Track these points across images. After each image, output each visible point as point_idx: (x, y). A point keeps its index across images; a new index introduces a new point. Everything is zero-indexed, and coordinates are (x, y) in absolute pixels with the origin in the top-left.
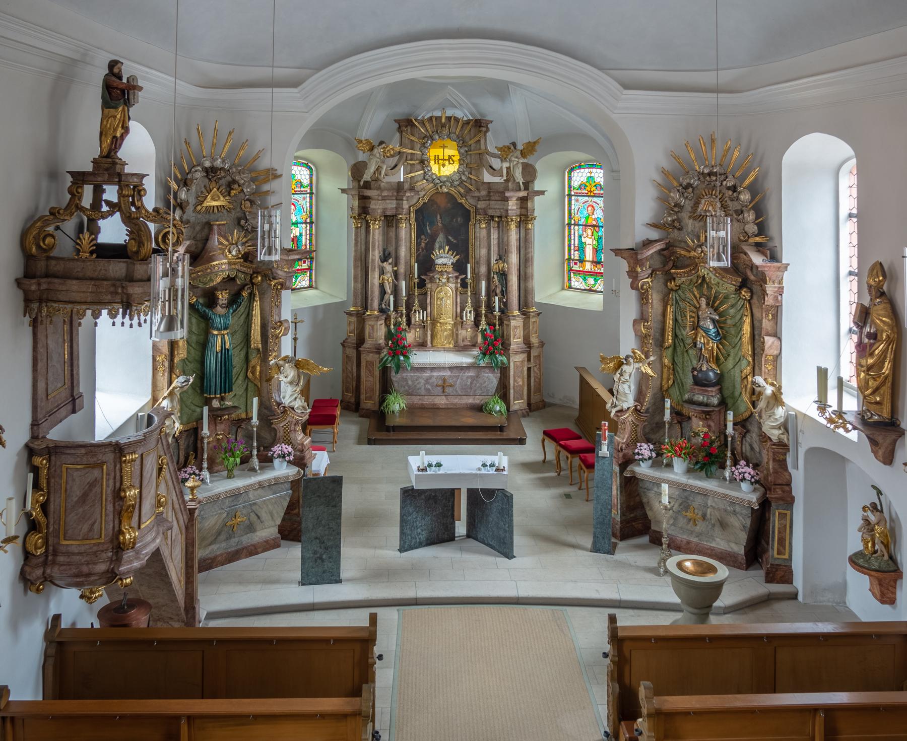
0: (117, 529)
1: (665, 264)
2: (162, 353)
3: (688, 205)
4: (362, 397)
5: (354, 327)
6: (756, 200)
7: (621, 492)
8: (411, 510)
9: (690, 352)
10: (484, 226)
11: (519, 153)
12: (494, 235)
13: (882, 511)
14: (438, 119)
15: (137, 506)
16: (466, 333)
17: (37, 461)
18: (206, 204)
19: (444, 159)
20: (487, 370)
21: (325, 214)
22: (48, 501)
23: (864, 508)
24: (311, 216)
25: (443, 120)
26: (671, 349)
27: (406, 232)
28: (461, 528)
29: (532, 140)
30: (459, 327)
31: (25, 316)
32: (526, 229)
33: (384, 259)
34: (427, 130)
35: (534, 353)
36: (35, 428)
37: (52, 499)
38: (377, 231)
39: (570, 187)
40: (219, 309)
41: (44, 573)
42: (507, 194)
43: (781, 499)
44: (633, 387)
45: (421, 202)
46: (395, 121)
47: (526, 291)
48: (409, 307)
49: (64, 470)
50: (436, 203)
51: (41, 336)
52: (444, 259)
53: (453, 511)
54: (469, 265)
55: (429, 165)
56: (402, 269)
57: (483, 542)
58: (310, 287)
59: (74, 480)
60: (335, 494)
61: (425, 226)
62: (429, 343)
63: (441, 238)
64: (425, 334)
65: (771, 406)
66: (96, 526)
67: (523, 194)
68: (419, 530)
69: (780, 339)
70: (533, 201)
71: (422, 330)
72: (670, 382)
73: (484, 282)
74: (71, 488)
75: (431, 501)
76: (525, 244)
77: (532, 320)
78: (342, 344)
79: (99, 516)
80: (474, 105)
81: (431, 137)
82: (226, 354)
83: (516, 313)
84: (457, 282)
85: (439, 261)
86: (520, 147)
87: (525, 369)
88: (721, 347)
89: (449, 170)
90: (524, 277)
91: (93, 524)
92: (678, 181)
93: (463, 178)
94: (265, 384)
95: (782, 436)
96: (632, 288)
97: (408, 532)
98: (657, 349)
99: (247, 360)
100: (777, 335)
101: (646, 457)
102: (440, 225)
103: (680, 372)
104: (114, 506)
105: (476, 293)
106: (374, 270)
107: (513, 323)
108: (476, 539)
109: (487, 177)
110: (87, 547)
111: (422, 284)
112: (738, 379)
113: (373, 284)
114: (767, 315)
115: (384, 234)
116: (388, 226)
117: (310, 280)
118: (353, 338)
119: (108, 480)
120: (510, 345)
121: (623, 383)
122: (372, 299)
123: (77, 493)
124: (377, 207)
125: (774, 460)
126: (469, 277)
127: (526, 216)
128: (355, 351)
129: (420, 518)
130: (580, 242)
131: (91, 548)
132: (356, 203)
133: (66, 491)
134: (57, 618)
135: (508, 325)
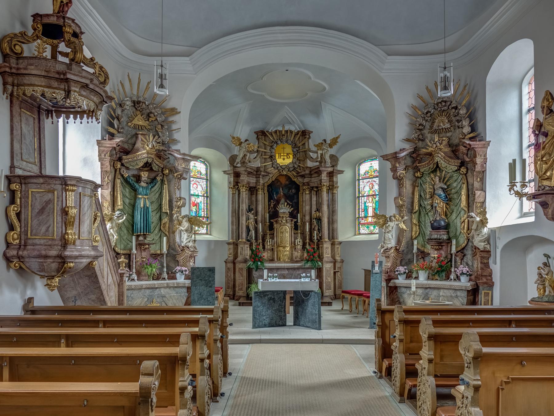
0: (64, 232)
1: (413, 162)
2: (106, 201)
3: (428, 125)
4: (237, 289)
5: (232, 251)
6: (470, 111)
7: (387, 298)
8: (259, 304)
9: (429, 214)
10: (307, 192)
11: (328, 145)
12: (314, 199)
13: (549, 266)
15: (77, 218)
16: (297, 254)
17: (14, 186)
18: (133, 122)
21: (215, 192)
22: (20, 211)
23: (539, 268)
24: (207, 193)
25: (283, 133)
26: (418, 213)
27: (262, 197)
28: (290, 319)
30: (294, 250)
31: (4, 94)
32: (333, 194)
33: (250, 210)
34: (274, 139)
35: (338, 265)
36: (12, 169)
37: (23, 211)
39: (359, 174)
40: (143, 184)
41: (17, 253)
42: (321, 169)
43: (485, 283)
44: (394, 236)
45: (271, 181)
46: (255, 132)
47: (333, 230)
48: (264, 240)
49: (30, 192)
50: (280, 181)
51: (16, 125)
52: (284, 209)
53: (285, 308)
54: (299, 215)
56: (259, 218)
57: (303, 326)
58: (207, 234)
59: (36, 199)
60: (211, 279)
62: (276, 259)
63: (283, 200)
65: (479, 228)
66: (51, 228)
67: (330, 169)
68: (264, 318)
69: (485, 192)
70: (337, 177)
72: (418, 234)
73: (308, 224)
74: (34, 204)
76: (332, 203)
77: (336, 246)
79: (52, 223)
80: (302, 122)
81: (276, 143)
82: (146, 209)
83: (327, 240)
84: (292, 224)
85: (281, 211)
86: (328, 142)
87: (332, 272)
88: (448, 207)
89: (288, 161)
90: (332, 221)
91: (49, 227)
92: (421, 112)
93: (296, 166)
94: (171, 235)
95: (486, 246)
96: (394, 179)
97: (257, 317)
98: (409, 215)
99: (160, 219)
100: (483, 189)
101: (402, 272)
102: (282, 194)
103: (423, 227)
104: (62, 219)
106: (242, 215)
107: (325, 245)
108: (300, 326)
109: (310, 164)
110: (45, 241)
111: (271, 227)
112: (459, 224)
113: (242, 224)
114: (477, 179)
115: (249, 199)
116: (251, 194)
117: (207, 229)
118: (231, 258)
119: (58, 201)
121: (388, 232)
122: (242, 233)
123: (38, 207)
124: (244, 178)
125: (481, 263)
126: (299, 221)
127: (333, 186)
128: (232, 264)
129: (265, 310)
130: (365, 206)
131: (47, 242)
132: (232, 179)
133: (31, 206)
134: (30, 300)
135: (321, 247)
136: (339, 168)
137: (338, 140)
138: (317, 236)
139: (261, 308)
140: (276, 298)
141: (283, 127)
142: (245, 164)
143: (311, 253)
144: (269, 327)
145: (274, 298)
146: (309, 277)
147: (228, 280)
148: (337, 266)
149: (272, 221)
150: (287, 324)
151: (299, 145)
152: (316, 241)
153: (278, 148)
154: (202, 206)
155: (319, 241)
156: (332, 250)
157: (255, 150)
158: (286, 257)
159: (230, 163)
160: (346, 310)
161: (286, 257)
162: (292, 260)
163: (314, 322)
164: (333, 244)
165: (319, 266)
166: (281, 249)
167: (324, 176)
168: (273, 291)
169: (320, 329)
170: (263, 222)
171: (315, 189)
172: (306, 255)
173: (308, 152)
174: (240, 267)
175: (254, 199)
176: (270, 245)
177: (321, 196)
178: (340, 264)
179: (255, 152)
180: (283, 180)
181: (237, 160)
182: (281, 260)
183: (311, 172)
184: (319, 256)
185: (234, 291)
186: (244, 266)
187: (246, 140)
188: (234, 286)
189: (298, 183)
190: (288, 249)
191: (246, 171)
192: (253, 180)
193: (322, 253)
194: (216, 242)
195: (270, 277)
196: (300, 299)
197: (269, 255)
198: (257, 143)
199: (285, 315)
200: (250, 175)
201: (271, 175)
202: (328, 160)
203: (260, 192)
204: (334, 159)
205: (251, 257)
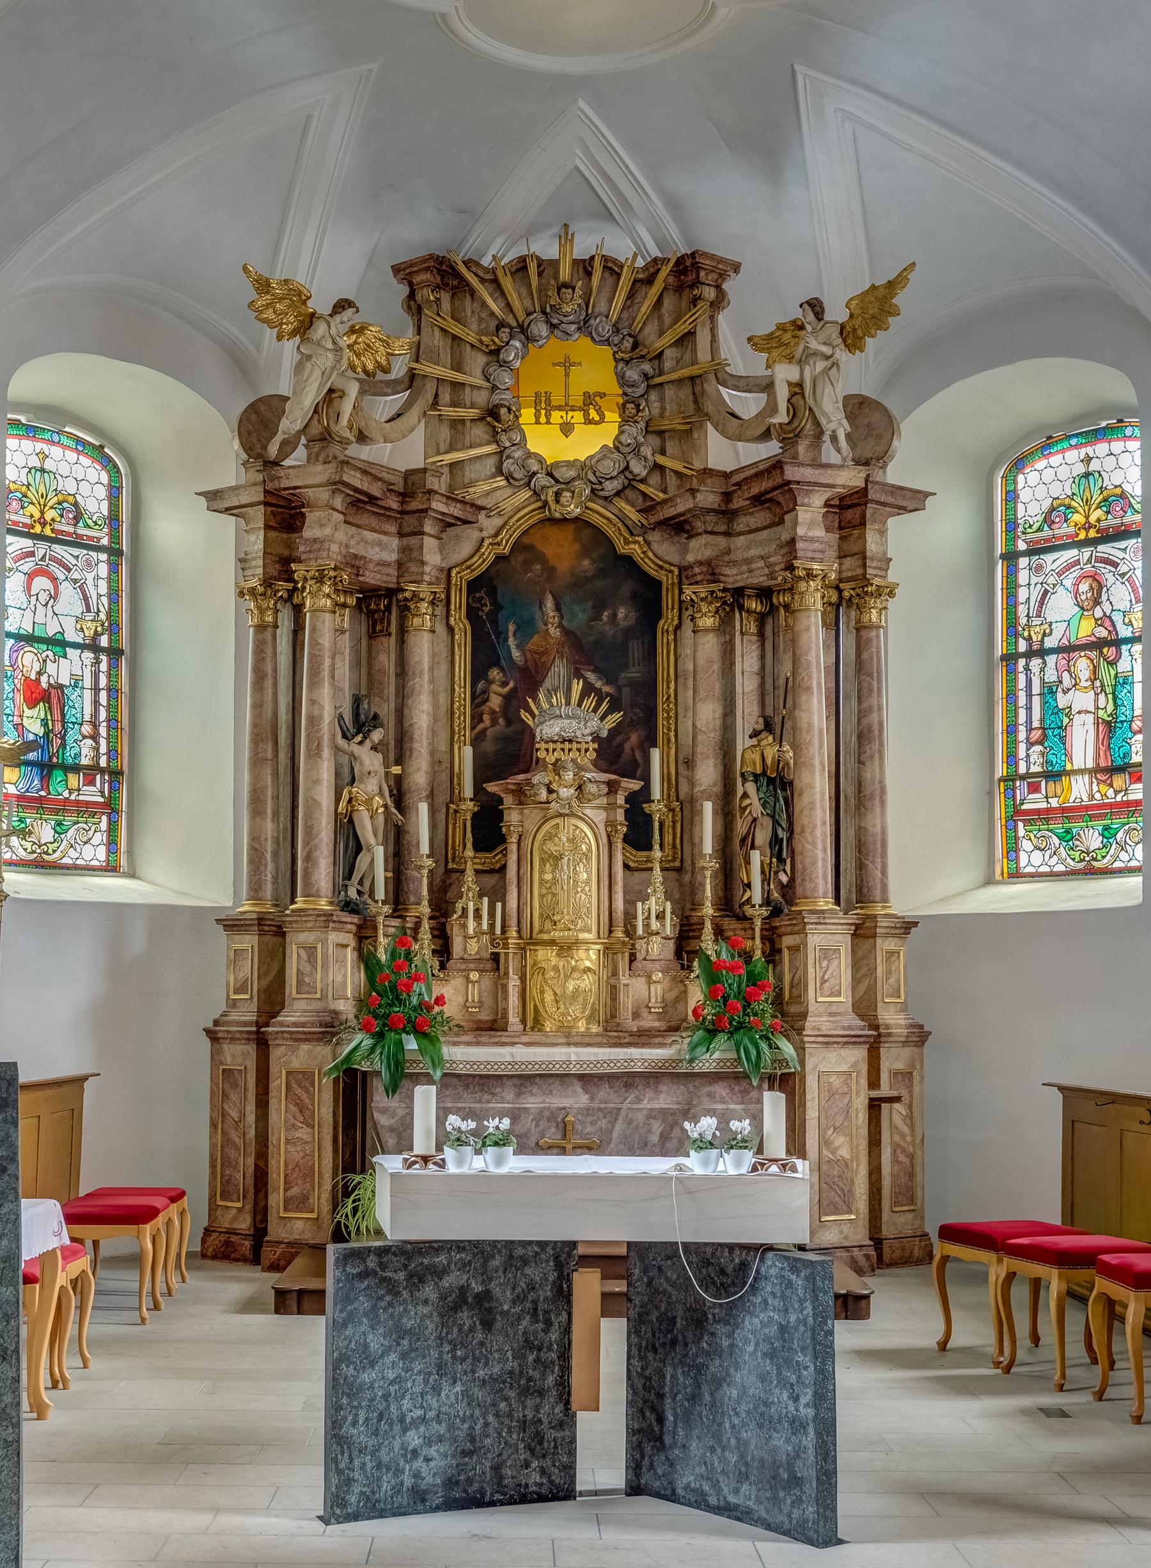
4: (276, 1200)
5: (248, 969)
8: (375, 1342)
10: (708, 622)
11: (834, 332)
12: (747, 661)
14: (546, 267)
16: (646, 990)
19: (567, 407)
20: (721, 1089)
24: (113, 628)
27: (433, 650)
28: (601, 1441)
29: (880, 281)
30: (623, 963)
33: (360, 724)
34: (509, 307)
35: (892, 1059)
38: (330, 627)
39: (1011, 526)
42: (791, 473)
45: (488, 555)
46: (396, 270)
47: (861, 846)
48: (442, 908)
50: (542, 559)
52: (568, 720)
54: (656, 754)
55: (516, 426)
56: (419, 774)
57: (700, 1502)
58: (110, 869)
61: (501, 635)
62: (514, 1019)
63: (559, 670)
64: (500, 988)
67: (850, 478)
68: (414, 1439)
71: (487, 981)
73: (708, 808)
75: (465, 1317)
76: (857, 679)
77: (884, 945)
78: (209, 1033)
80: (674, 205)
81: (523, 329)
83: (825, 903)
84: (611, 807)
86: (837, 312)
87: (860, 1103)
90: (854, 798)
93: (638, 468)
97: (359, 1434)
102: (554, 632)
105: (680, 870)
106: (315, 753)
107: (816, 939)
108: (672, 1497)
109: (721, 452)
111: (489, 830)
113: (313, 804)
115: (356, 664)
116: (373, 635)
118: (247, 1013)
120: (804, 1015)
122: (308, 858)
124: (328, 532)
126: (656, 794)
128: (251, 1049)
129: (416, 1384)
132: (256, 542)
136: (898, 472)
137: (901, 299)
138: (766, 880)
139: (391, 1367)
140: (504, 1296)
141: (566, 237)
142: (335, 449)
143: (731, 982)
144: (452, 1504)
145: (485, 1297)
146: (743, 1144)
147: (227, 1142)
148: (886, 1066)
149: (492, 787)
150: (584, 1480)
151: (659, 344)
152: (758, 913)
153: (534, 367)
154: (81, 704)
155: (776, 912)
156: (856, 965)
157: (399, 370)
158: (575, 1010)
159: (247, 447)
160: (970, 1355)
161: (575, 1010)
162: (614, 1031)
163: (781, 1479)
164: (863, 933)
165: (783, 1062)
166: (546, 956)
167: (810, 521)
168: (476, 1244)
169: (830, 1540)
170: (442, 798)
171: (753, 605)
172: (696, 994)
173: (711, 386)
174: (296, 1064)
175: (386, 660)
176: (479, 933)
177: (794, 642)
178: (907, 1052)
179: (394, 387)
180: (562, 552)
181: (284, 424)
182: (549, 1026)
183: (727, 496)
184: (778, 1002)
185: (261, 1214)
186: (319, 1059)
187: (342, 305)
188: (261, 1178)
189: (650, 568)
190: (589, 957)
191: (337, 485)
192: (379, 549)
193: (800, 985)
194: (161, 917)
195: (460, 1142)
196: (684, 1299)
197: (474, 993)
198: (410, 335)
199: (567, 1421)
200: (364, 519)
201: (489, 524)
202: (835, 420)
203: (424, 618)
204: (871, 422)
205: (361, 1003)
